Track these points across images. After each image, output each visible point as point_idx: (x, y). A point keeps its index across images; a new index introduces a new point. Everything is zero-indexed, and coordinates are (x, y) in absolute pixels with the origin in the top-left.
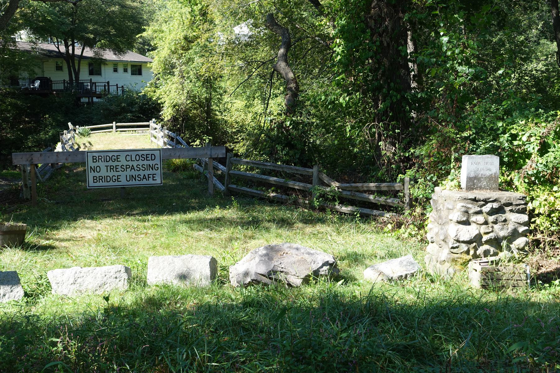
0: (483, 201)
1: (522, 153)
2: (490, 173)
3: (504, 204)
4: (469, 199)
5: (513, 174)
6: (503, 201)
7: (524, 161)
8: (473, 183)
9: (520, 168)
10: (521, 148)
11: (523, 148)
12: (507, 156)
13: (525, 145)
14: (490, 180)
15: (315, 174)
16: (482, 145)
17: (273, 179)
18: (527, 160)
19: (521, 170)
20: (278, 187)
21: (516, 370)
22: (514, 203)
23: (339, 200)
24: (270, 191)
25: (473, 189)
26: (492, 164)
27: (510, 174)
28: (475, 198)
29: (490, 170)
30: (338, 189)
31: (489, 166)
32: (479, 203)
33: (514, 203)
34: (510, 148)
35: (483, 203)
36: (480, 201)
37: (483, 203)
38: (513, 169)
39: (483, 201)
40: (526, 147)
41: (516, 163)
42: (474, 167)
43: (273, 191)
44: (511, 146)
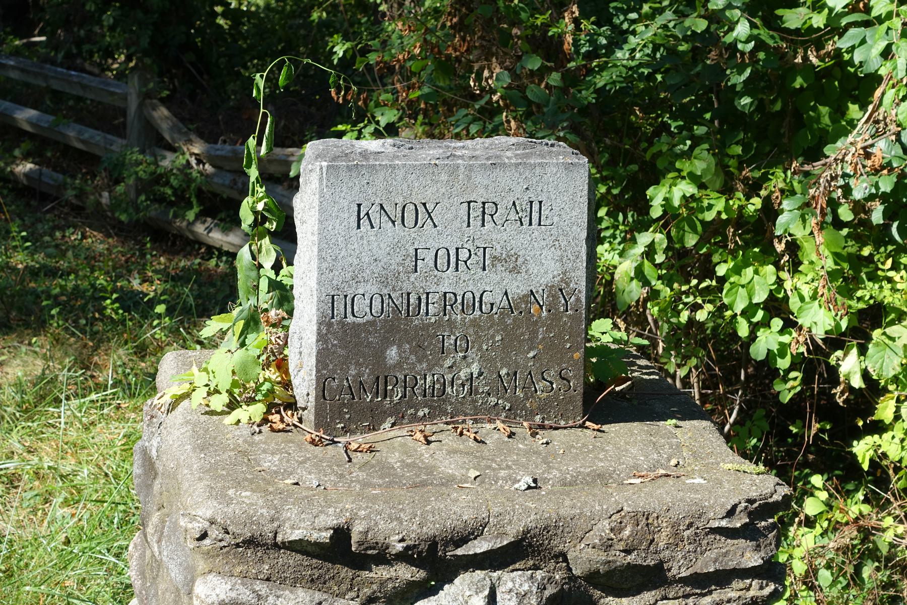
0: (405, 557)
1: (826, 73)
2: (517, 287)
3: (593, 578)
4: (299, 547)
5: (778, 180)
6: (584, 557)
7: (839, 112)
8: (376, 375)
9: (815, 154)
10: (819, 46)
11: (829, 47)
12: (749, 87)
13: (842, 32)
14: (511, 342)
15: (133, 104)
16: (640, 28)
17: (25, 116)
18: (853, 110)
19: (816, 167)
20: (40, 145)
21: (904, 8)
22: (679, 569)
23: (201, 201)
24: (17, 152)
25: (372, 419)
26: (530, 213)
27: (765, 178)
28: (341, 534)
29: (512, 263)
30: (199, 162)
31: (503, 236)
32: (381, 572)
33: (679, 569)
34: (760, 45)
35: (405, 573)
36: (383, 557)
37: (405, 573)
38: (781, 159)
39: (405, 557)
40: (843, 44)
41: (798, 119)
42: (382, 244)
43: (26, 157)
44: (764, 34)
